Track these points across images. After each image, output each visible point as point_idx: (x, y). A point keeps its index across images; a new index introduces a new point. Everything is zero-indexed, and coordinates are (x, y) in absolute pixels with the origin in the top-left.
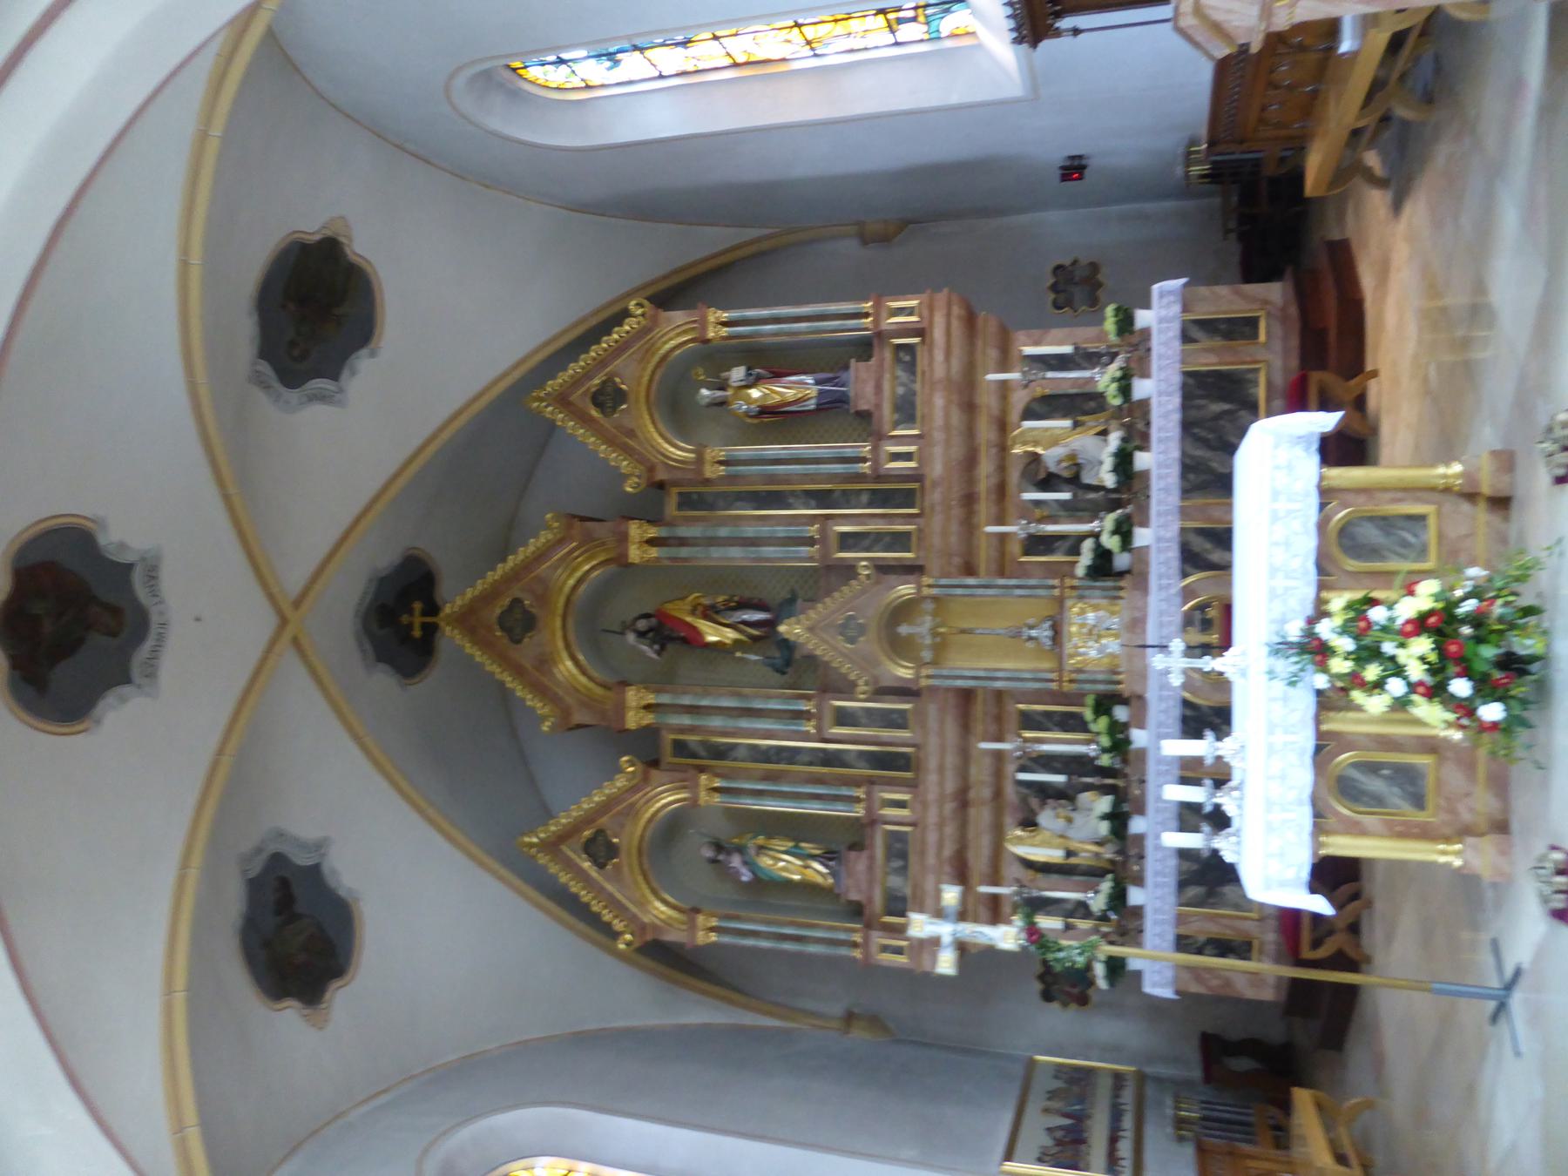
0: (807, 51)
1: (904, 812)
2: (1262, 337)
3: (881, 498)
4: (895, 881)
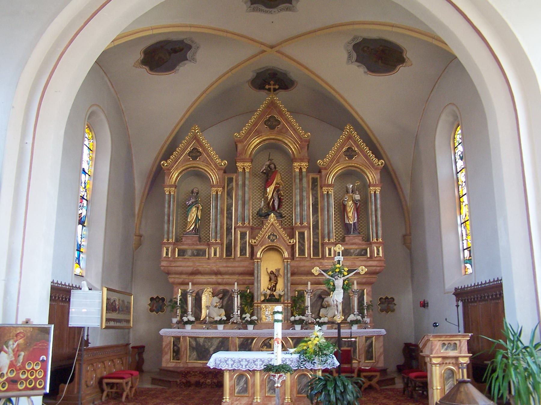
0: (463, 221)
1: (213, 255)
2: (367, 361)
4: (189, 253)
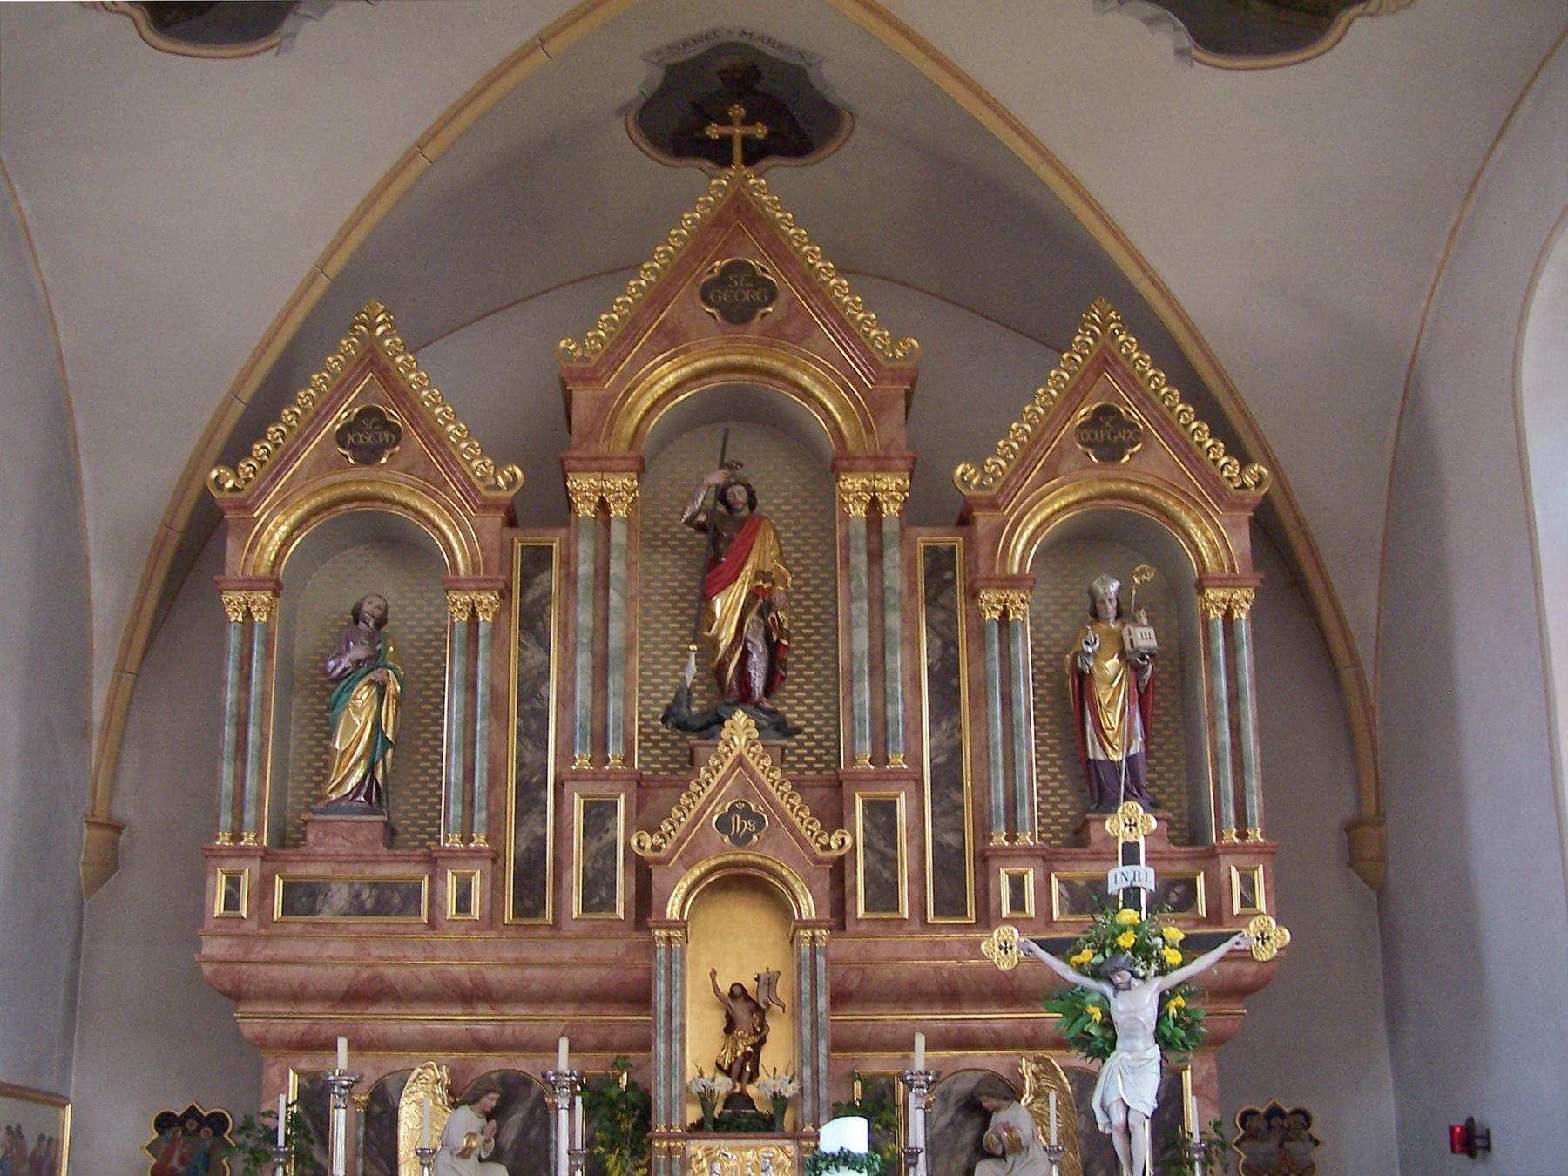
3: (949, 864)
4: (340, 896)
